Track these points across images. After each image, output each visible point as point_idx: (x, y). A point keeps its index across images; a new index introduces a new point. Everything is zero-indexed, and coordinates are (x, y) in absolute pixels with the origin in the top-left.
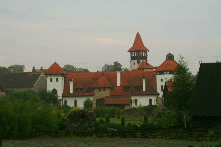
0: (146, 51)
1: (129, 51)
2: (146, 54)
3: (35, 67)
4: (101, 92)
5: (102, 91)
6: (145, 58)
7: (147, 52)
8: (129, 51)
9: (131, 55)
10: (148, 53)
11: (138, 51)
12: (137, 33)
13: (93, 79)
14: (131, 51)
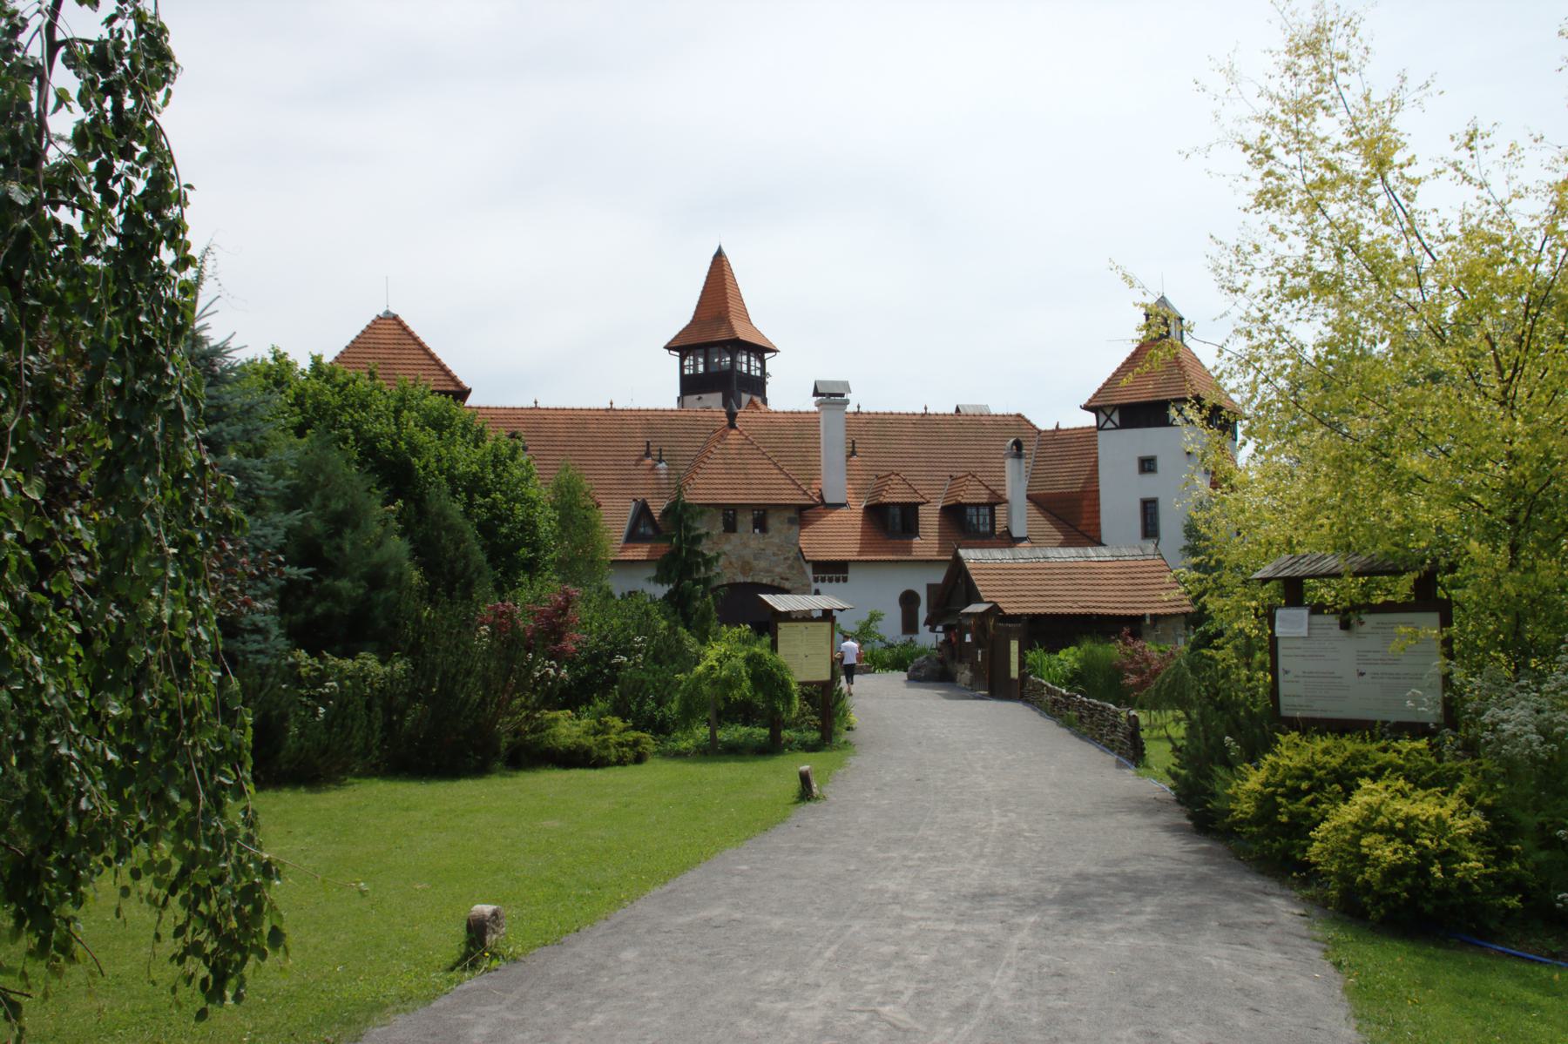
0: (760, 351)
1: (669, 347)
2: (763, 368)
3: (762, 309)
4: (734, 537)
5: (740, 528)
6: (757, 386)
7: (767, 355)
8: (669, 347)
9: (682, 368)
10: (771, 362)
11: (719, 351)
12: (715, 251)
13: (648, 454)
14: (682, 346)
